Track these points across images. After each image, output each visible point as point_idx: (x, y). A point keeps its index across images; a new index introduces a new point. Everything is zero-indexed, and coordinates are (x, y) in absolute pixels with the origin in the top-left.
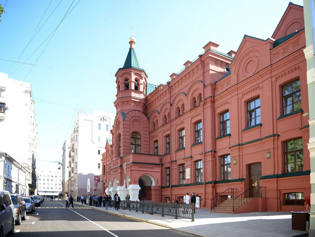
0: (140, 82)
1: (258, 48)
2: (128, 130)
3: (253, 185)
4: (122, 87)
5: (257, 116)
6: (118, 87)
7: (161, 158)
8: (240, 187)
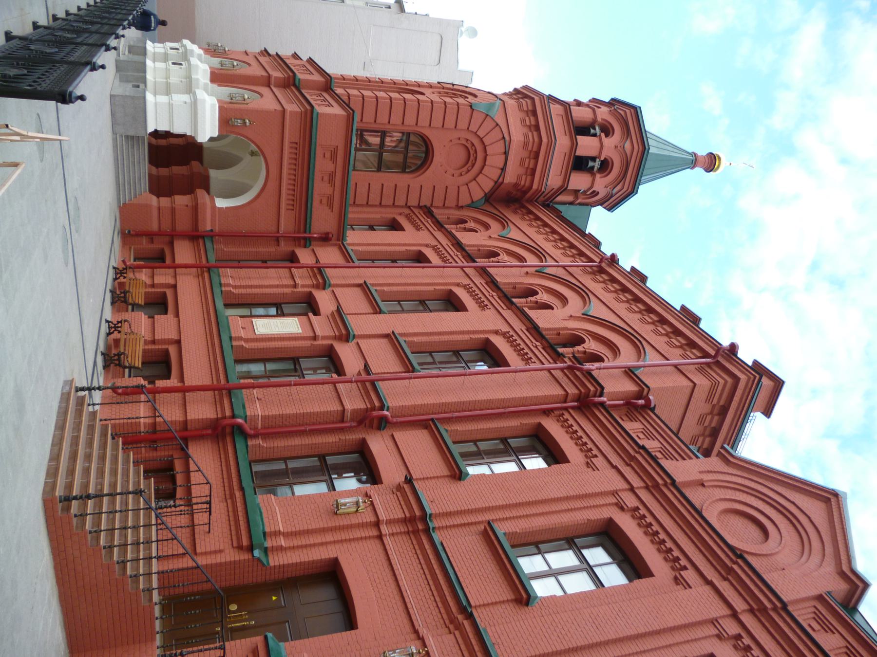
0: (598, 176)
1: (815, 543)
2: (437, 122)
3: (234, 607)
4: (581, 115)
5: (562, 578)
7: (334, 238)
8: (216, 546)
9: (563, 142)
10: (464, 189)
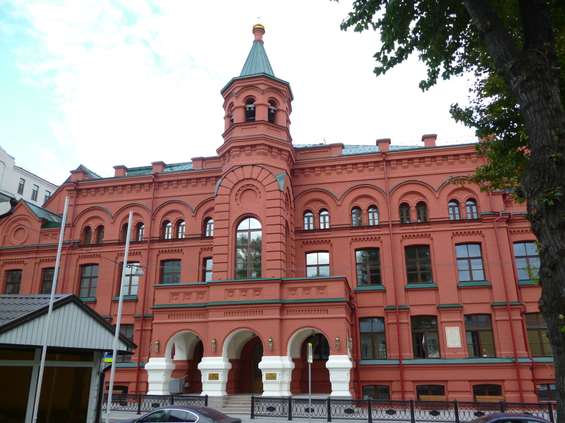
0: (279, 107)
4: (239, 116)
9: (260, 130)
10: (268, 188)
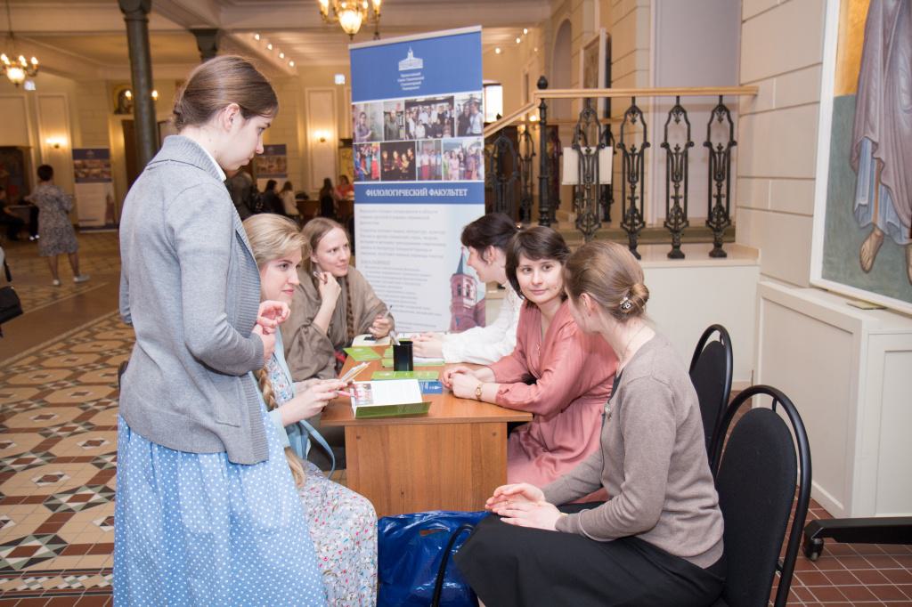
4: (456, 293)
6: (453, 292)
